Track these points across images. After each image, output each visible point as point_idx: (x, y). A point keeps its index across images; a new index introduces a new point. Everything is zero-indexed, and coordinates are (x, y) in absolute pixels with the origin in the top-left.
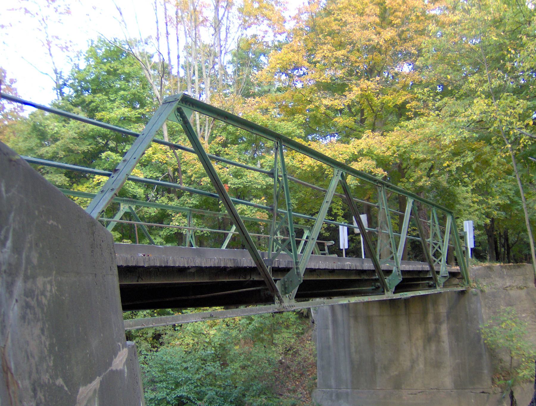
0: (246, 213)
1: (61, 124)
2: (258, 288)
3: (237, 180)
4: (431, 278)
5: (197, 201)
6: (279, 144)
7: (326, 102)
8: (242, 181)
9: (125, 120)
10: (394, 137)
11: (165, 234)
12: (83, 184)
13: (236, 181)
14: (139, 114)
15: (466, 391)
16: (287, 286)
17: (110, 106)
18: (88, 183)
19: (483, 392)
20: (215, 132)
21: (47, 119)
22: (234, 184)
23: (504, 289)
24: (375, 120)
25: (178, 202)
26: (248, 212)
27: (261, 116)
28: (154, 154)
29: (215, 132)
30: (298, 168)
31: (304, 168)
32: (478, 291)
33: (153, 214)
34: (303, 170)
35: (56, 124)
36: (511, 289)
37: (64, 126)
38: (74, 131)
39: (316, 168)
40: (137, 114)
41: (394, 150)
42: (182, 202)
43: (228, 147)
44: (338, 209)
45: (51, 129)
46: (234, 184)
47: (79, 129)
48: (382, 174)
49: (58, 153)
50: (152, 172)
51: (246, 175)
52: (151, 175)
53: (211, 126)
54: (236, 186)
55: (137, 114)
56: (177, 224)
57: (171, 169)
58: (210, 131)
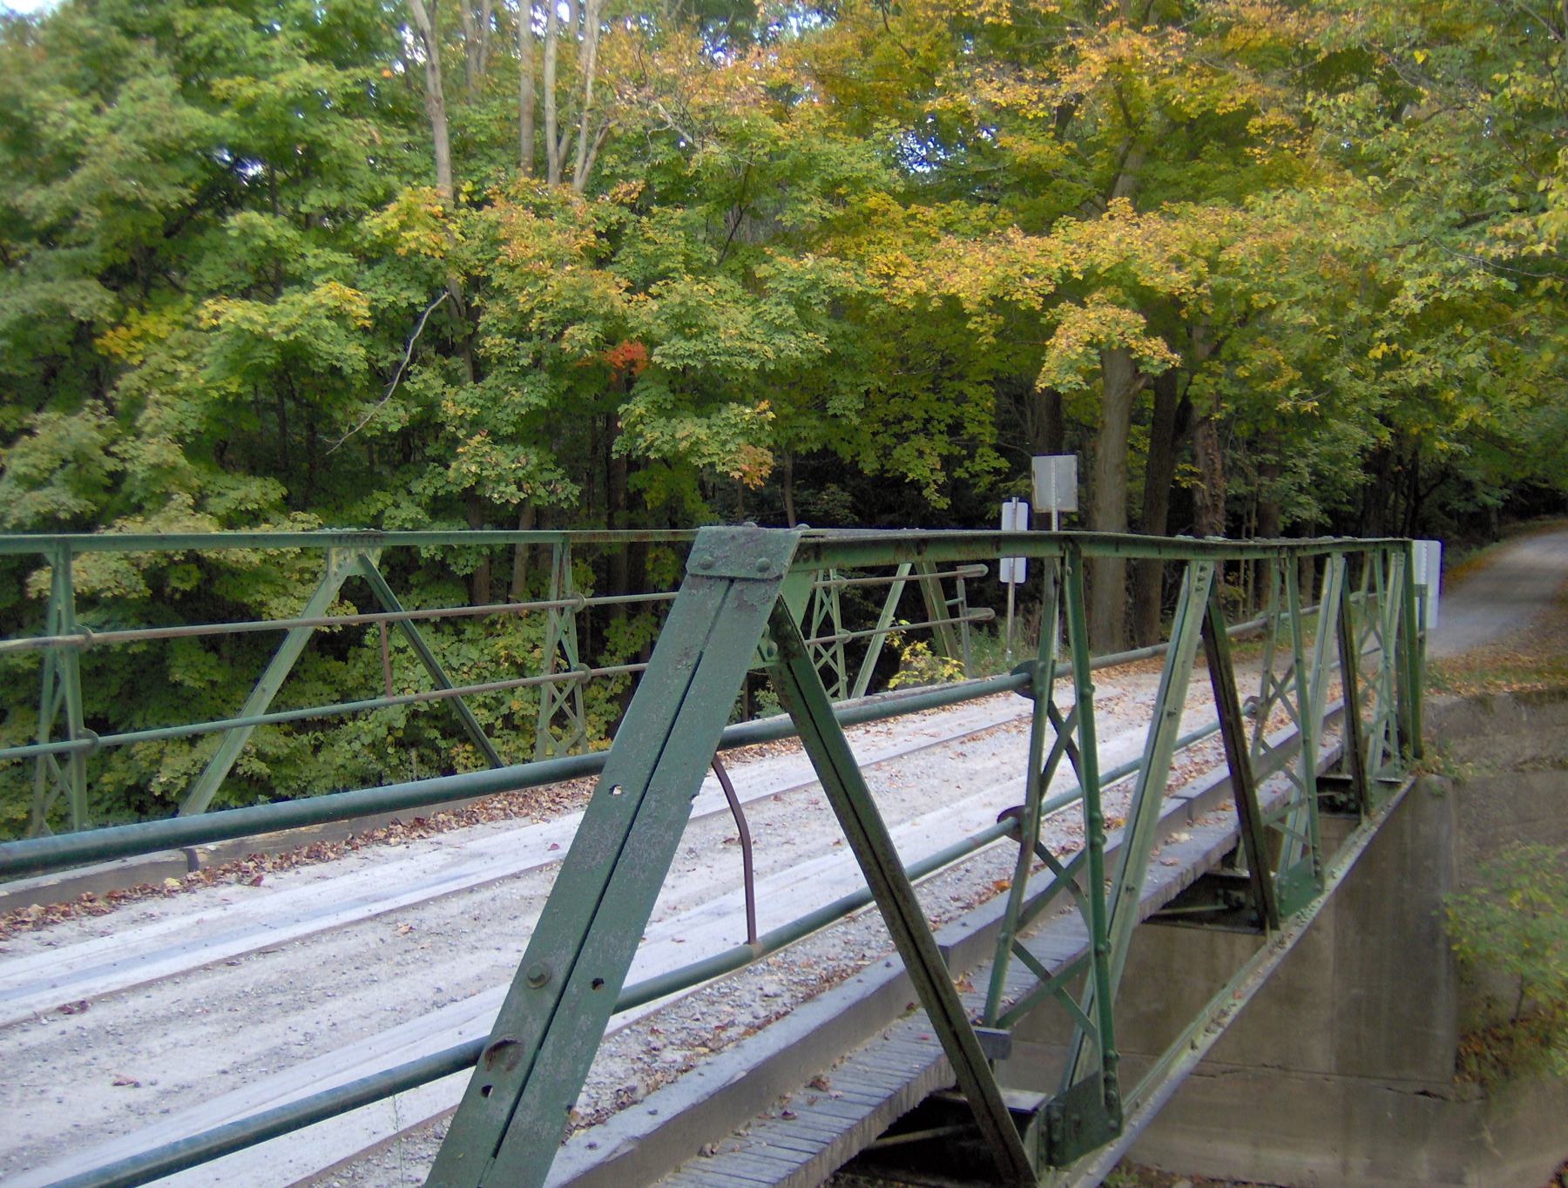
0: (705, 450)
1: (86, 105)
2: (941, 1131)
3: (683, 343)
4: (1346, 783)
5: (544, 397)
6: (1068, 568)
7: (989, 92)
8: (700, 346)
9: (310, 101)
10: (1204, 231)
11: (430, 491)
12: (159, 311)
13: (681, 345)
14: (356, 84)
15: (1373, 1082)
16: (1056, 1137)
17: (259, 49)
18: (178, 309)
19: (1424, 1093)
20: (610, 160)
21: (39, 84)
22: (674, 358)
23: (1516, 770)
24: (1129, 148)
25: (478, 392)
26: (714, 448)
27: (771, 121)
28: (404, 226)
29: (610, 160)
30: (875, 299)
31: (896, 301)
32: (1448, 785)
33: (395, 428)
34: (890, 305)
35: (71, 106)
36: (1535, 769)
37: (97, 110)
38: (133, 136)
39: (936, 303)
40: (349, 82)
41: (1199, 274)
42: (490, 394)
43: (651, 216)
44: (981, 423)
45: (55, 124)
46: (674, 358)
47: (150, 128)
48: (1164, 361)
49: (76, 214)
50: (395, 288)
51: (716, 328)
52: (391, 299)
53: (598, 139)
54: (679, 364)
55: (349, 82)
56: (473, 469)
57: (457, 278)
58: (593, 154)
